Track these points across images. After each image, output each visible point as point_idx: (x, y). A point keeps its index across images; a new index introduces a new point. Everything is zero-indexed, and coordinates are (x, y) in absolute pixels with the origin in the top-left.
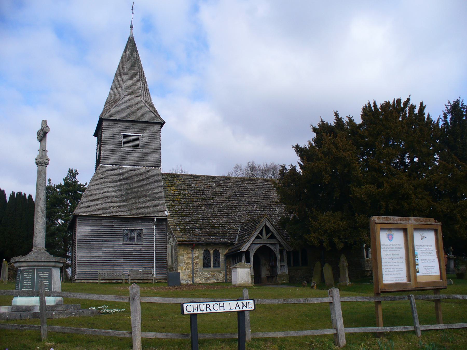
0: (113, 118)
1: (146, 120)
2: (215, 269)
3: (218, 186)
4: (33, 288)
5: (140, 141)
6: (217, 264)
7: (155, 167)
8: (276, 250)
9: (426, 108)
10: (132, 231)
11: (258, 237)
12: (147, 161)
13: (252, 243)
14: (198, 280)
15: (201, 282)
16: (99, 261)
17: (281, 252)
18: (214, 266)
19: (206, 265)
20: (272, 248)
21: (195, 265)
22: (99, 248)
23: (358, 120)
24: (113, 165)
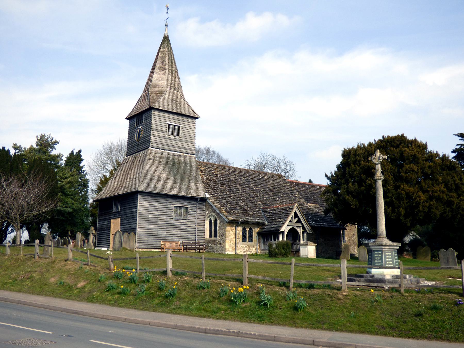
0: (161, 108)
1: (185, 113)
2: (250, 243)
3: (230, 174)
4: (393, 263)
5: (181, 131)
6: (251, 240)
7: (191, 154)
8: (300, 231)
9: (428, 145)
10: (180, 207)
11: (290, 221)
12: (185, 149)
14: (238, 252)
15: (241, 253)
16: (154, 232)
17: (303, 233)
18: (249, 241)
19: (244, 240)
20: (298, 230)
21: (237, 240)
22: (155, 221)
23: (451, 156)
24: (165, 150)
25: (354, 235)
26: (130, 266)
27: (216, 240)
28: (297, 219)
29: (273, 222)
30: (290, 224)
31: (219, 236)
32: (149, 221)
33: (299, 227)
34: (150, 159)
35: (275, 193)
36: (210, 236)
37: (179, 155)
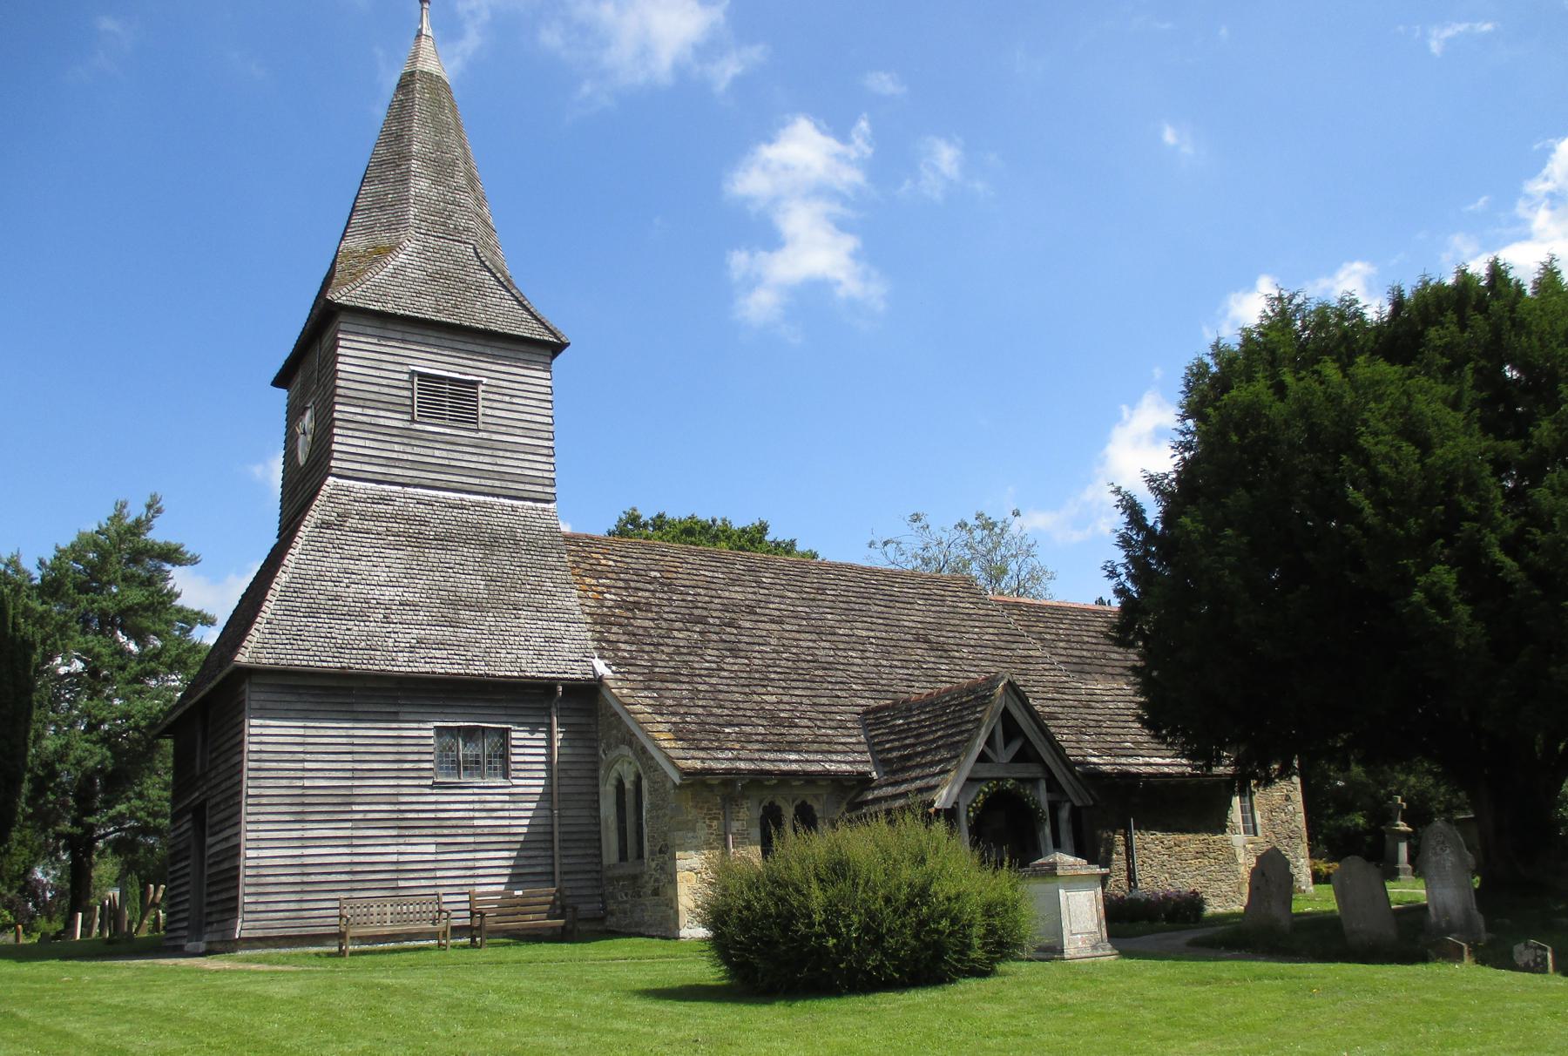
0: (377, 307)
11: (983, 758)
12: (501, 476)
13: (969, 779)
25: (1288, 798)
26: (1448, 864)
27: (642, 873)
28: (1016, 746)
29: (904, 769)
30: (985, 771)
31: (652, 853)
32: (303, 807)
33: (1033, 781)
34: (326, 525)
35: (934, 647)
36: (623, 856)
37: (478, 504)
